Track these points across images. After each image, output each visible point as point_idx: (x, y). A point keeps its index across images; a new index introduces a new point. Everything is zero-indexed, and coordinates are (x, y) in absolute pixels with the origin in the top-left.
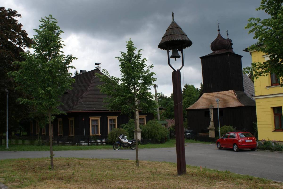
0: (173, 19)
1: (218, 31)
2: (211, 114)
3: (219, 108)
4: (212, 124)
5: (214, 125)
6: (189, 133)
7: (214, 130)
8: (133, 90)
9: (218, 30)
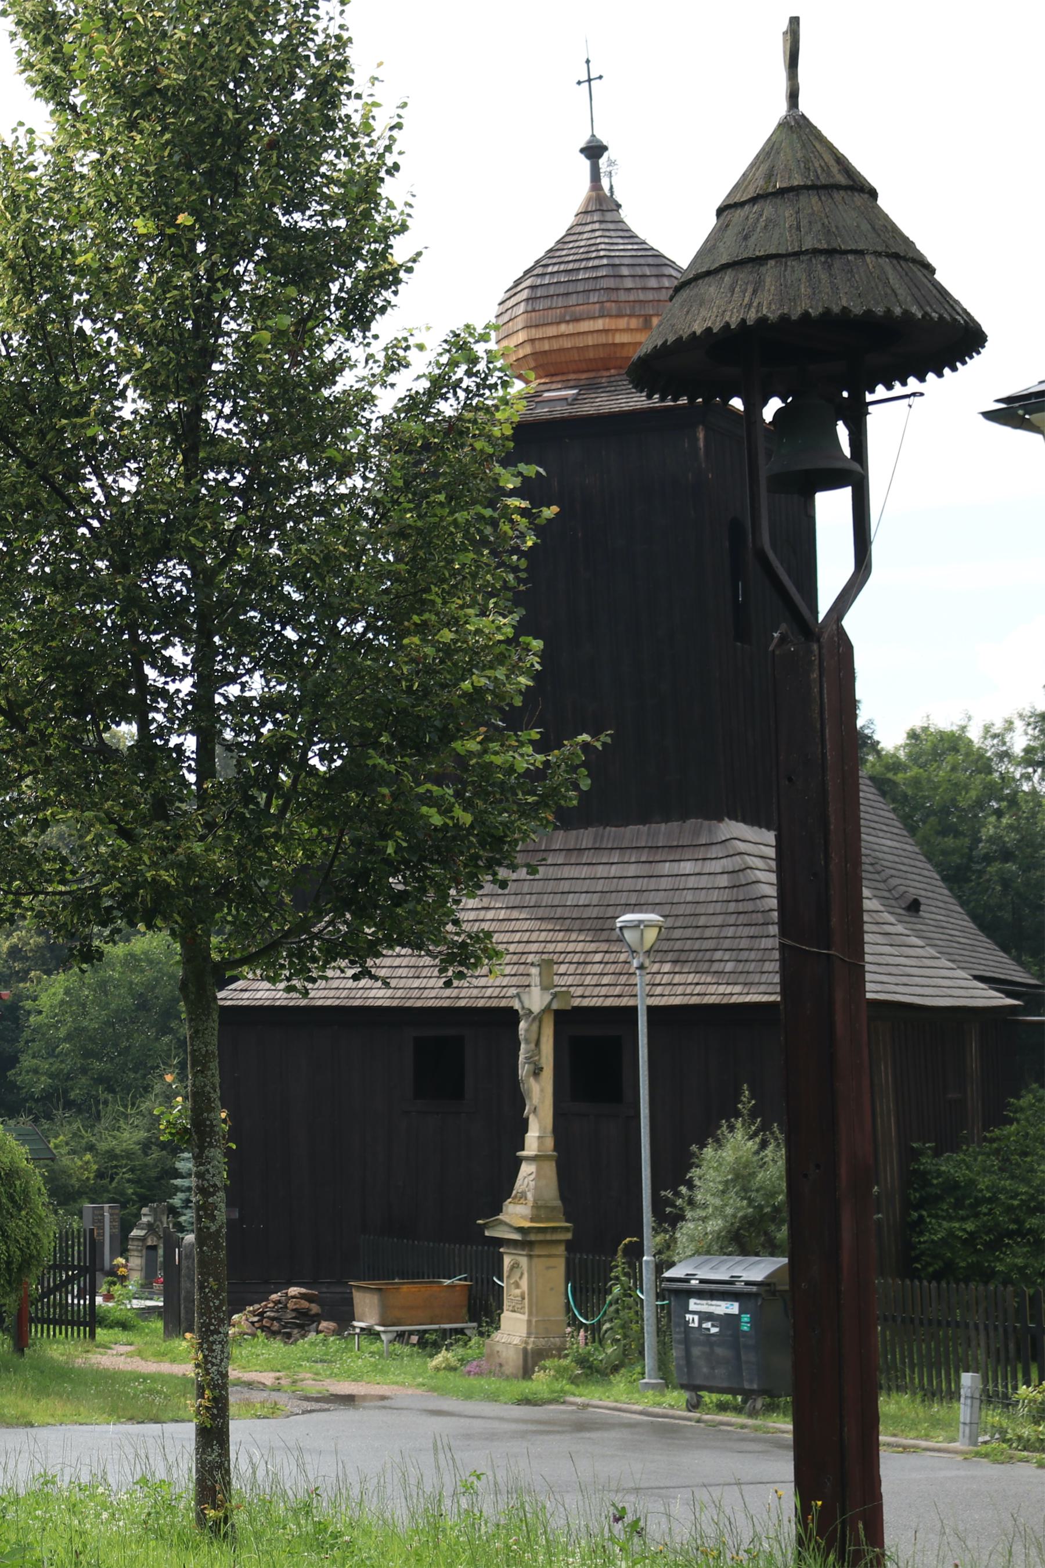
0: (793, 97)
1: (586, 164)
2: (537, 1072)
3: (651, 1010)
4: (533, 1180)
5: (563, 1196)
6: (734, 1308)
7: (561, 1250)
8: (385, 900)
9: (582, 144)
